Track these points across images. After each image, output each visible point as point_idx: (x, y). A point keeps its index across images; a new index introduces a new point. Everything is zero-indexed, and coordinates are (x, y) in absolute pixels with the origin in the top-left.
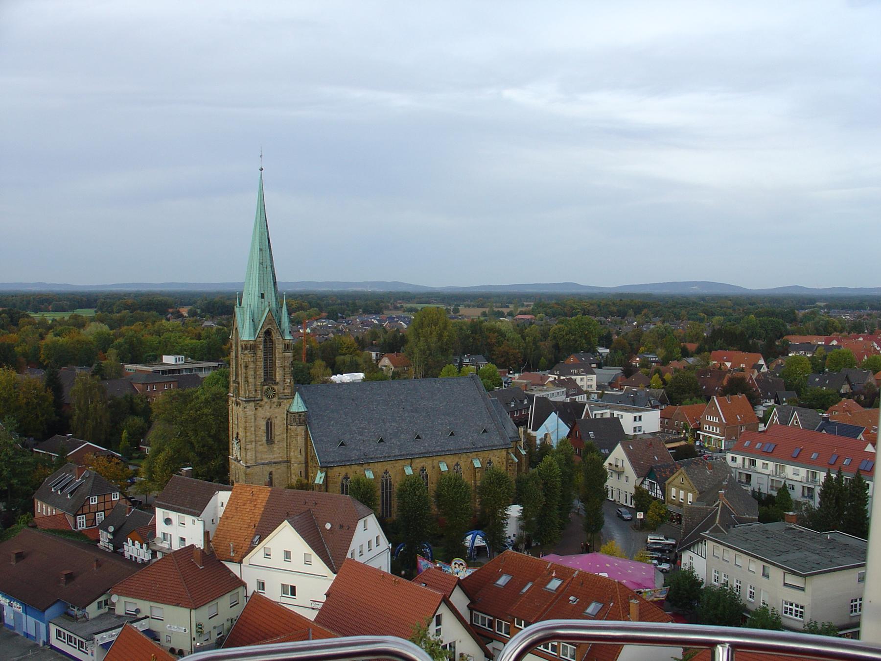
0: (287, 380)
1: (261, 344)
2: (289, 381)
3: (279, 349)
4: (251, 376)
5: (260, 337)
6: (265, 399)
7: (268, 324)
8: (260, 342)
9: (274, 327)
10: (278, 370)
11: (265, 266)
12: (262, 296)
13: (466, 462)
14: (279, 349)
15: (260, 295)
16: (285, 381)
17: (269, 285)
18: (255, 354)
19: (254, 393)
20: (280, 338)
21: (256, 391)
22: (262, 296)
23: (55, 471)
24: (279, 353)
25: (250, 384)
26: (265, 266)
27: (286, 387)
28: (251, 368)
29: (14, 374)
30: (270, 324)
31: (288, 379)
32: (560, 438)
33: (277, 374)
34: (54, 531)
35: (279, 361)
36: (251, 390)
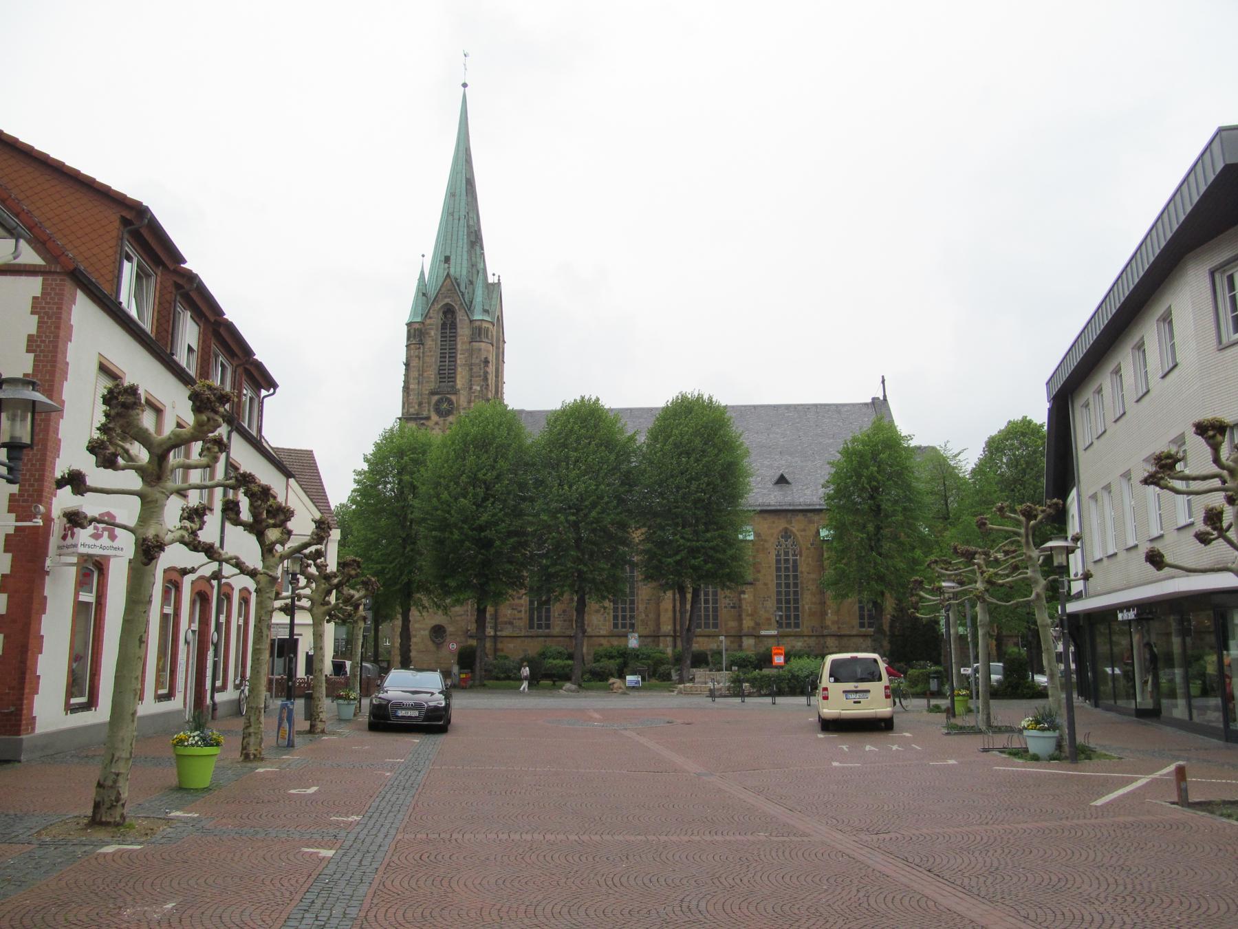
0: (474, 387)
1: (432, 329)
2: (478, 388)
3: (463, 336)
4: (414, 379)
5: (430, 318)
6: (435, 418)
7: (445, 297)
8: (430, 325)
9: (455, 301)
10: (459, 369)
11: (456, 216)
12: (447, 259)
13: (804, 530)
14: (463, 336)
15: (443, 259)
16: (471, 388)
17: (460, 243)
18: (423, 344)
19: (417, 407)
20: (466, 318)
21: (420, 404)
22: (447, 259)
23: (1097, 500)
24: (463, 343)
25: (411, 393)
26: (456, 216)
27: (473, 398)
28: (414, 367)
29: (969, 549)
30: (449, 297)
31: (478, 385)
32: (206, 560)
33: (458, 377)
34: (762, 512)
35: (462, 356)
36: (412, 403)
